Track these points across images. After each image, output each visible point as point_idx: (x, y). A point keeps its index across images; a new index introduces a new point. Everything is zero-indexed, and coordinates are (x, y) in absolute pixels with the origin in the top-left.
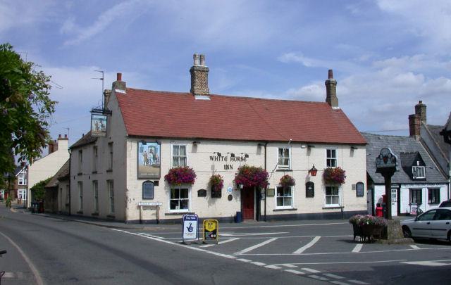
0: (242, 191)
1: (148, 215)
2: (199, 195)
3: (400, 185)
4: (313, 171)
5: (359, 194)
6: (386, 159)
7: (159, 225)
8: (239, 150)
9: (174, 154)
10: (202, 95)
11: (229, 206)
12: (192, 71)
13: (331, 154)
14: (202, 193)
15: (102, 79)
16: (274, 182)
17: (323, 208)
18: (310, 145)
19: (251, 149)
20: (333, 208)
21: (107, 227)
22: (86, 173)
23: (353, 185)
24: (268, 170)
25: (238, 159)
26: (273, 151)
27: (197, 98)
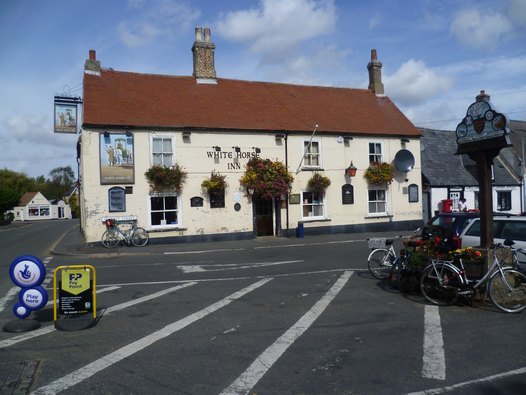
2: (352, 202)
3: (463, 187)
5: (413, 200)
8: (248, 142)
10: (207, 78)
11: (237, 217)
14: (196, 202)
16: (300, 185)
17: (366, 218)
18: (347, 137)
20: (378, 217)
26: (297, 144)
27: (199, 81)
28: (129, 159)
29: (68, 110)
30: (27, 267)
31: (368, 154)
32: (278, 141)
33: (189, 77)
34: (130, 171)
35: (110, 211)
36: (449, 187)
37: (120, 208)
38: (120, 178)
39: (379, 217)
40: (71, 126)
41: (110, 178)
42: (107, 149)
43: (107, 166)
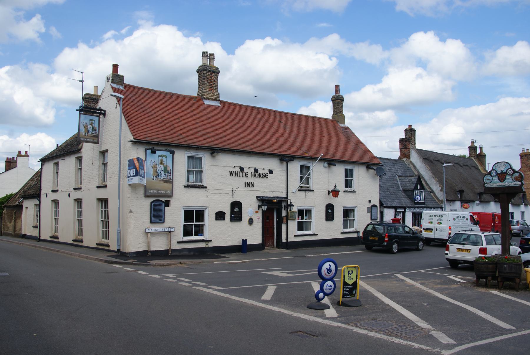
0: (263, 212)
2: (217, 219)
3: (405, 208)
10: (212, 99)
13: (348, 173)
15: (82, 81)
27: (207, 102)
29: (92, 120)
30: (330, 266)
33: (194, 97)
34: (169, 185)
36: (396, 208)
37: (160, 220)
40: (94, 136)
41: (153, 191)
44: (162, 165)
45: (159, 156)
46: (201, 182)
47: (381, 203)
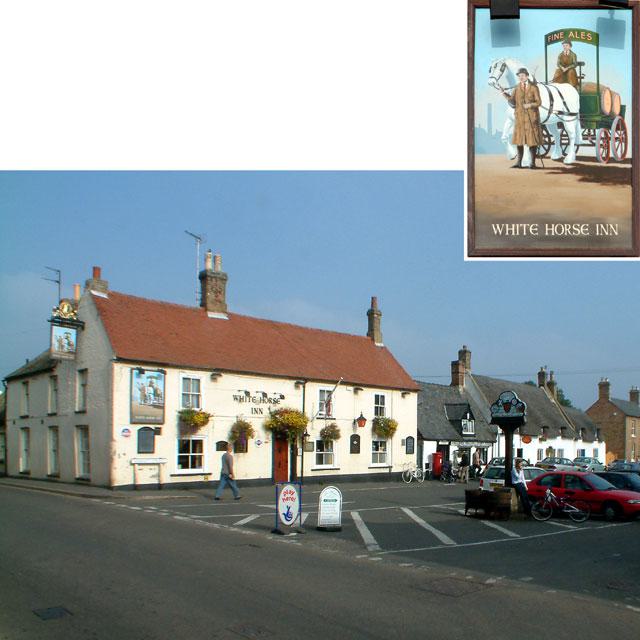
1: (146, 477)
2: (358, 452)
4: (361, 421)
5: (409, 451)
6: (507, 406)
7: (162, 491)
9: (184, 390)
12: (203, 277)
13: (379, 400)
18: (357, 387)
19: (286, 387)
21: (83, 496)
22: (36, 416)
23: (403, 441)
24: (308, 414)
25: (270, 401)
26: (313, 389)
27: (211, 315)
28: (613, 133)
31: (374, 405)
32: (297, 385)
34: (159, 411)
35: (139, 452)
38: (566, 230)
39: (380, 468)
41: (515, 229)
42: (504, 83)
43: (506, 170)
44: (151, 389)
45: (148, 378)
46: (198, 407)
47: (419, 434)
